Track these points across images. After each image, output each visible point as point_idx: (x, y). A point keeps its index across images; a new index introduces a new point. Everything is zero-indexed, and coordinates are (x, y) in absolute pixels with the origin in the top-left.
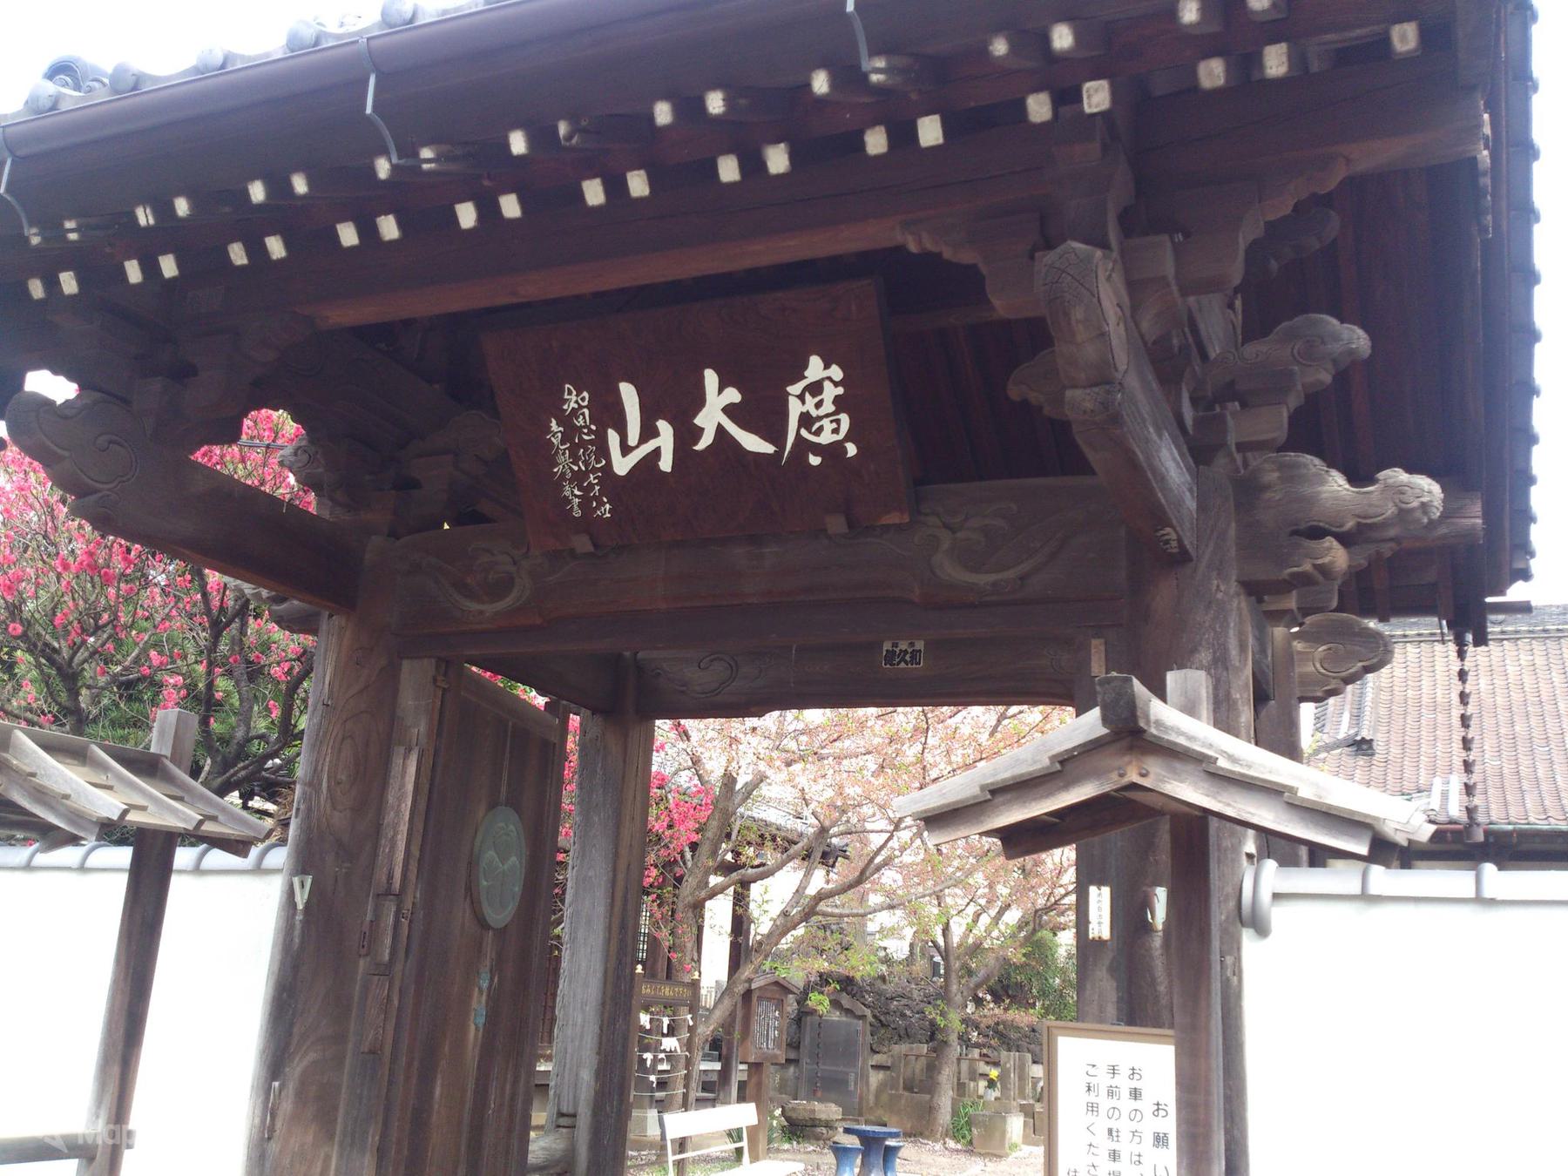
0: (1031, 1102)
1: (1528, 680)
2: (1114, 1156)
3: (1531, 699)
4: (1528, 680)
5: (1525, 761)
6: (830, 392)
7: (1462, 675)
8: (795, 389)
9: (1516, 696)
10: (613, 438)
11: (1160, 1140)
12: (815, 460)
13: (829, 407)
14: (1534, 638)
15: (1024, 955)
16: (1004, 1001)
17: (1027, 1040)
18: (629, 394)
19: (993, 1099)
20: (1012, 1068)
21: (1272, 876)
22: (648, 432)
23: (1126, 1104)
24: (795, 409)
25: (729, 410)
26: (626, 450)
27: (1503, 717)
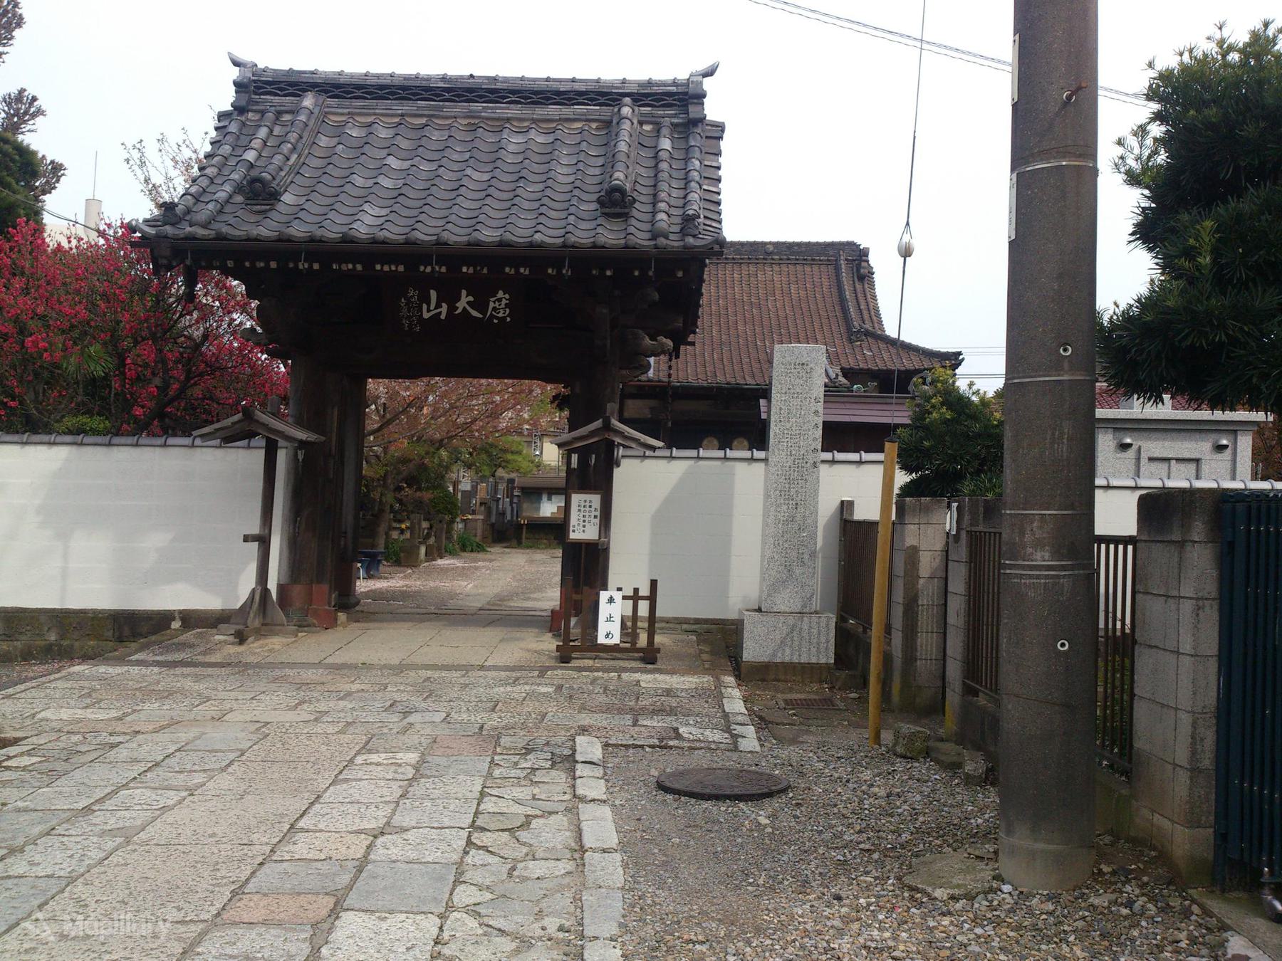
2: (584, 521)
6: (504, 302)
7: (670, 367)
8: (493, 299)
10: (425, 306)
11: (595, 517)
12: (495, 321)
13: (503, 306)
18: (433, 294)
21: (621, 451)
22: (438, 306)
23: (588, 509)
24: (492, 305)
25: (468, 303)
26: (429, 310)
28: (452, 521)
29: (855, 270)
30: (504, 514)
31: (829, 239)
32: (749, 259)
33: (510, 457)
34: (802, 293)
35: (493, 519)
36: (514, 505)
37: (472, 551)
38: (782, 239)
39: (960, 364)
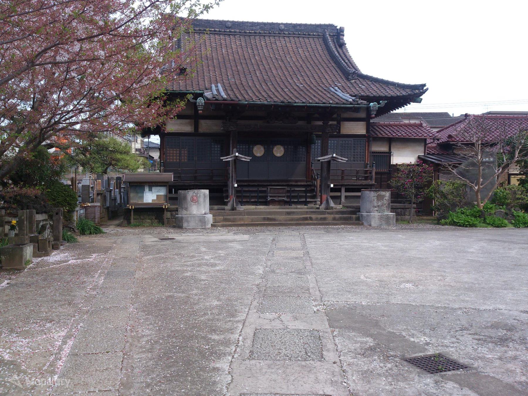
0: (36, 234)
1: (240, 50)
3: (242, 58)
4: (240, 50)
5: (243, 80)
9: (236, 56)
14: (241, 35)
15: (33, 156)
16: (20, 183)
17: (33, 202)
19: (14, 236)
20: (25, 218)
27: (233, 64)
28: (71, 211)
29: (335, 41)
30: (115, 199)
31: (318, 22)
32: (270, 33)
33: (119, 156)
34: (307, 54)
35: (108, 204)
36: (122, 194)
37: (90, 233)
38: (289, 22)
39: (424, 93)
